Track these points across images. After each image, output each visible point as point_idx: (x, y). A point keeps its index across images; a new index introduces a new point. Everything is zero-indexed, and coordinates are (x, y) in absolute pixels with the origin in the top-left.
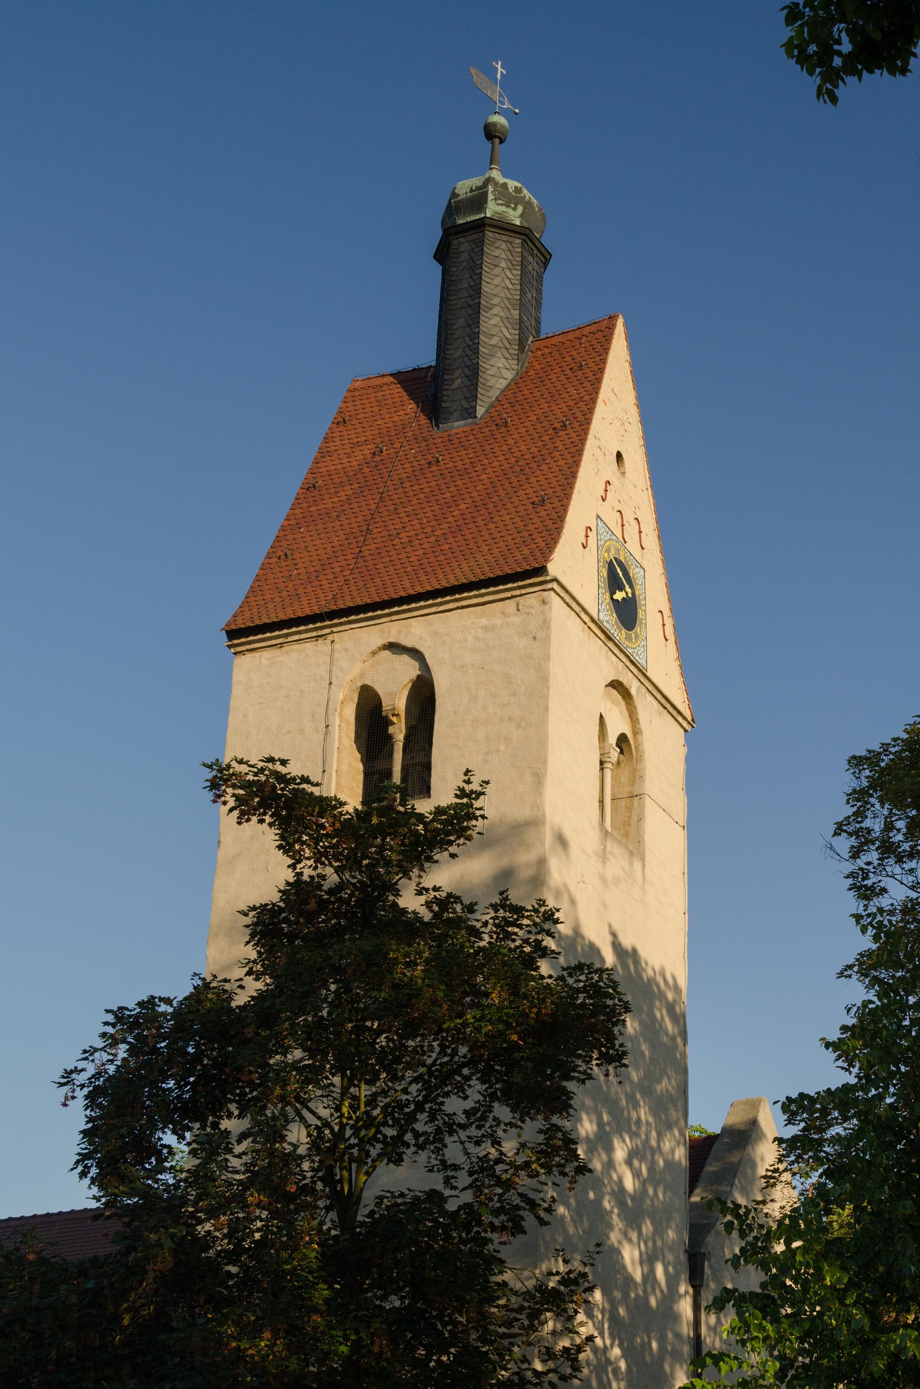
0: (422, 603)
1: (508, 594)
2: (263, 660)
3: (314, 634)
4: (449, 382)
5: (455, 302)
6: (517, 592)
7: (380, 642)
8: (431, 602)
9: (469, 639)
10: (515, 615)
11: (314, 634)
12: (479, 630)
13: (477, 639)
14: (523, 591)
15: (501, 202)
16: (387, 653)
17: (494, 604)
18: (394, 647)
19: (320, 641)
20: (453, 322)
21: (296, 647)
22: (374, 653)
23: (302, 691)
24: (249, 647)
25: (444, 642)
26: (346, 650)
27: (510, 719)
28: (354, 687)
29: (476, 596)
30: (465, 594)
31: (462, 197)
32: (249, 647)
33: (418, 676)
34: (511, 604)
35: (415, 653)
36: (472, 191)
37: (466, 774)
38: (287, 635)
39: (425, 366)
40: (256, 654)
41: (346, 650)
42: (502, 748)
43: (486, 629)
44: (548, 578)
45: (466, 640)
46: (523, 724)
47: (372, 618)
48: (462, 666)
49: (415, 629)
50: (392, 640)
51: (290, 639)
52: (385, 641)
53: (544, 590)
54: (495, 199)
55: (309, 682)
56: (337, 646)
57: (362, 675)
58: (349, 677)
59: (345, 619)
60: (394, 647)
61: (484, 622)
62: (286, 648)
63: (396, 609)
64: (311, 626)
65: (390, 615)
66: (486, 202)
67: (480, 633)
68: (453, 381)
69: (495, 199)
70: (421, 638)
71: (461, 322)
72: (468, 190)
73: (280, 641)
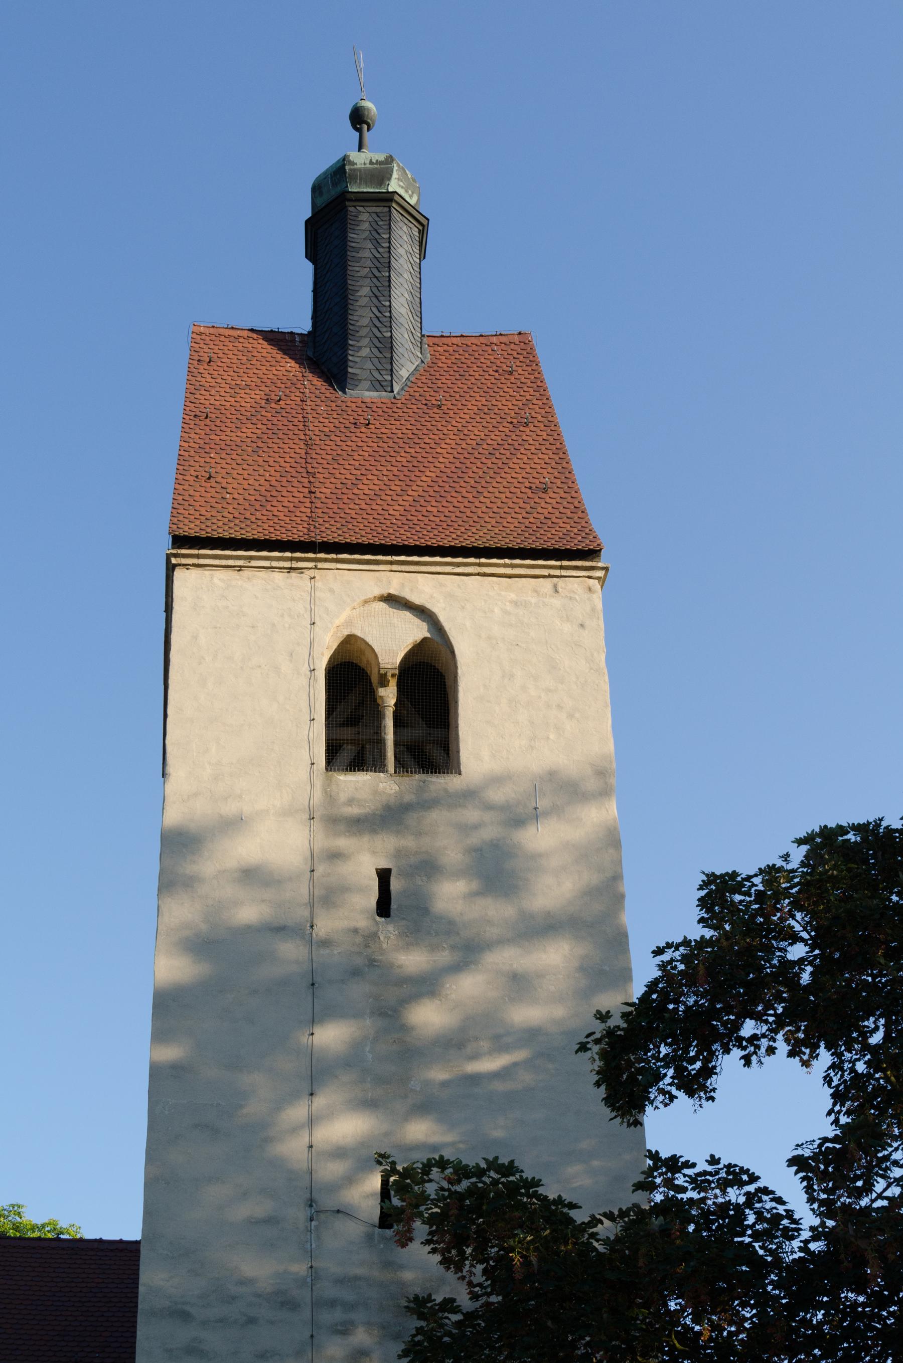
0: (438, 559)
1: (545, 572)
2: (216, 580)
3: (287, 564)
4: (356, 349)
5: (357, 269)
6: (557, 572)
7: (378, 591)
8: (449, 559)
9: (496, 610)
10: (552, 596)
11: (287, 564)
12: (508, 604)
13: (506, 613)
14: (564, 573)
15: (401, 184)
16: (383, 605)
17: (523, 579)
18: (391, 600)
19: (294, 574)
20: (357, 289)
21: (262, 574)
22: (366, 602)
23: (274, 625)
24: (195, 561)
25: (463, 608)
26: (332, 591)
27: (559, 707)
28: (339, 634)
29: (505, 566)
30: (494, 561)
31: (359, 166)
32: (195, 561)
33: (425, 639)
34: (547, 584)
35: (422, 612)
36: (371, 163)
37: (169, 883)
38: (251, 558)
39: (286, 330)
40: (207, 572)
41: (332, 591)
42: (552, 737)
43: (516, 604)
44: (600, 565)
45: (493, 611)
46: (577, 715)
47: (368, 562)
48: (489, 638)
49: (428, 585)
50: (392, 591)
51: (254, 563)
52: (385, 592)
53: (589, 577)
54: (399, 179)
55: (282, 616)
56: (319, 584)
57: (349, 622)
58: (338, 622)
59: (334, 556)
60: (391, 600)
61: (513, 596)
62: (246, 573)
63: (403, 558)
64: (288, 554)
65: (391, 563)
66: (389, 179)
67: (509, 607)
68: (360, 348)
69: (399, 179)
70: (432, 597)
71: (365, 291)
72: (368, 162)
73: (241, 563)
